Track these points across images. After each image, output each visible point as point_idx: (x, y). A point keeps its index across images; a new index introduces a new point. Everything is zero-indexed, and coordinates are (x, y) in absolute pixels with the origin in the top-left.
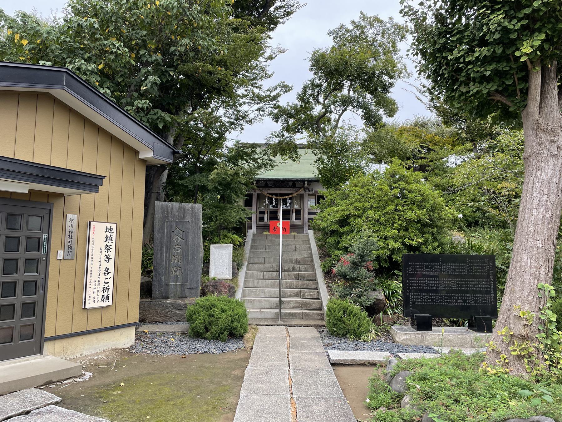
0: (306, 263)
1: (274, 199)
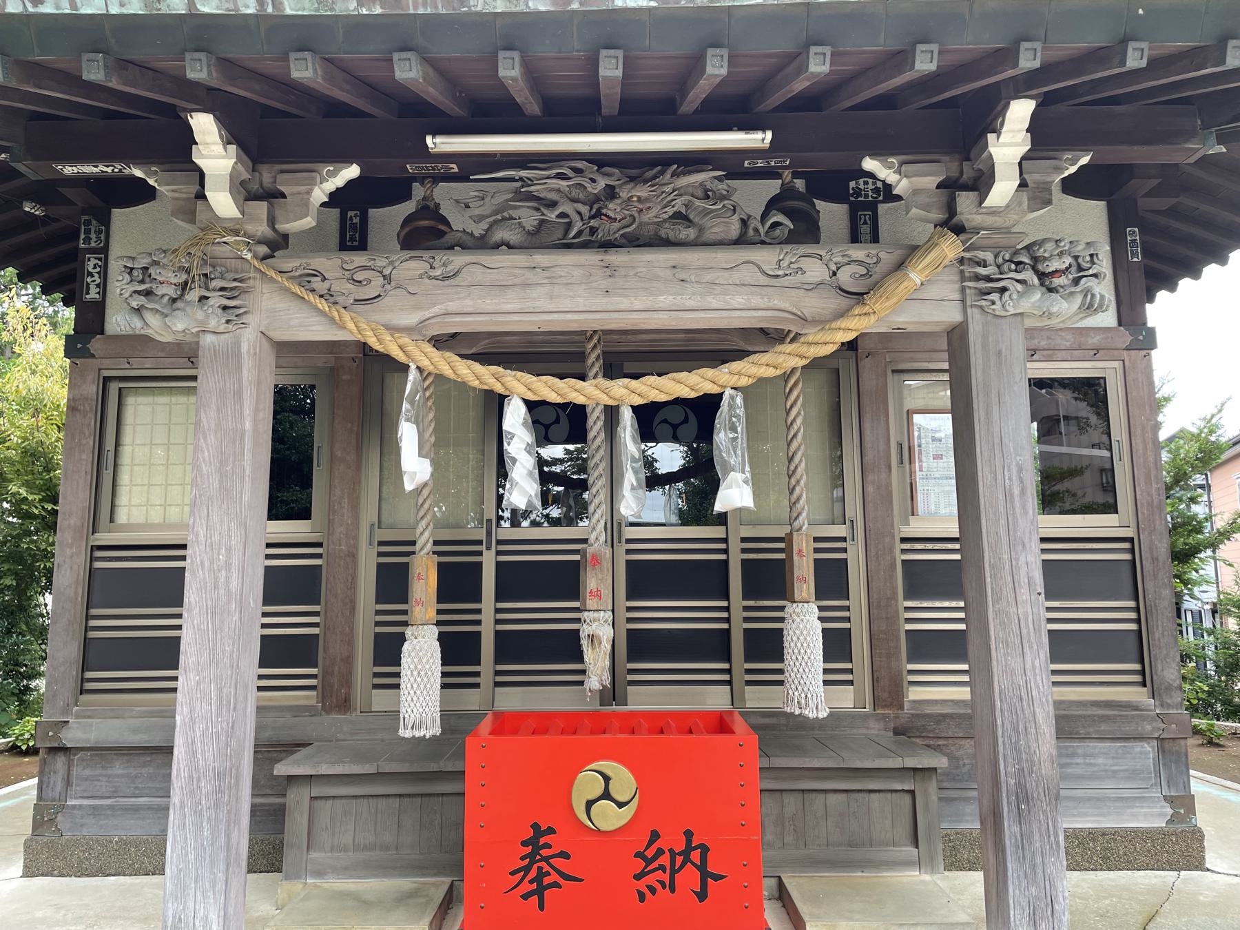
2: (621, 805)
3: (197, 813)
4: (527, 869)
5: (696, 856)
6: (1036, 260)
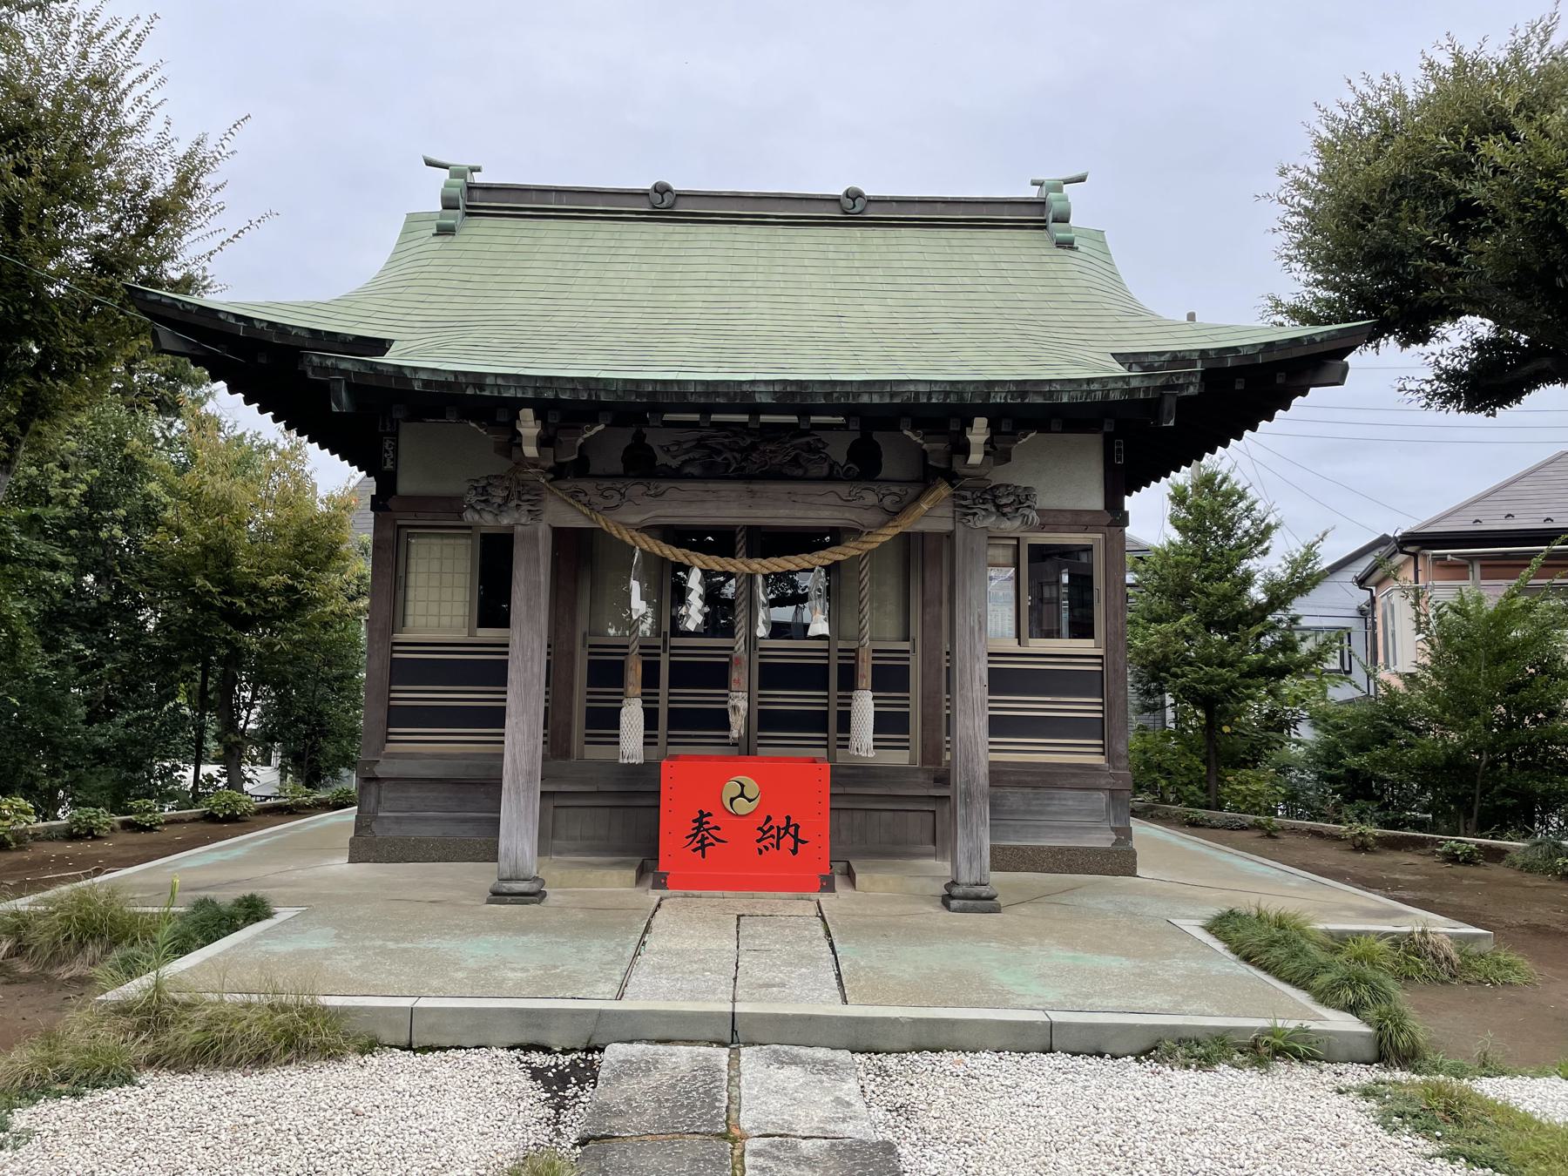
1: (694, 581)
2: (750, 801)
3: (517, 793)
4: (695, 835)
5: (792, 830)
6: (995, 497)
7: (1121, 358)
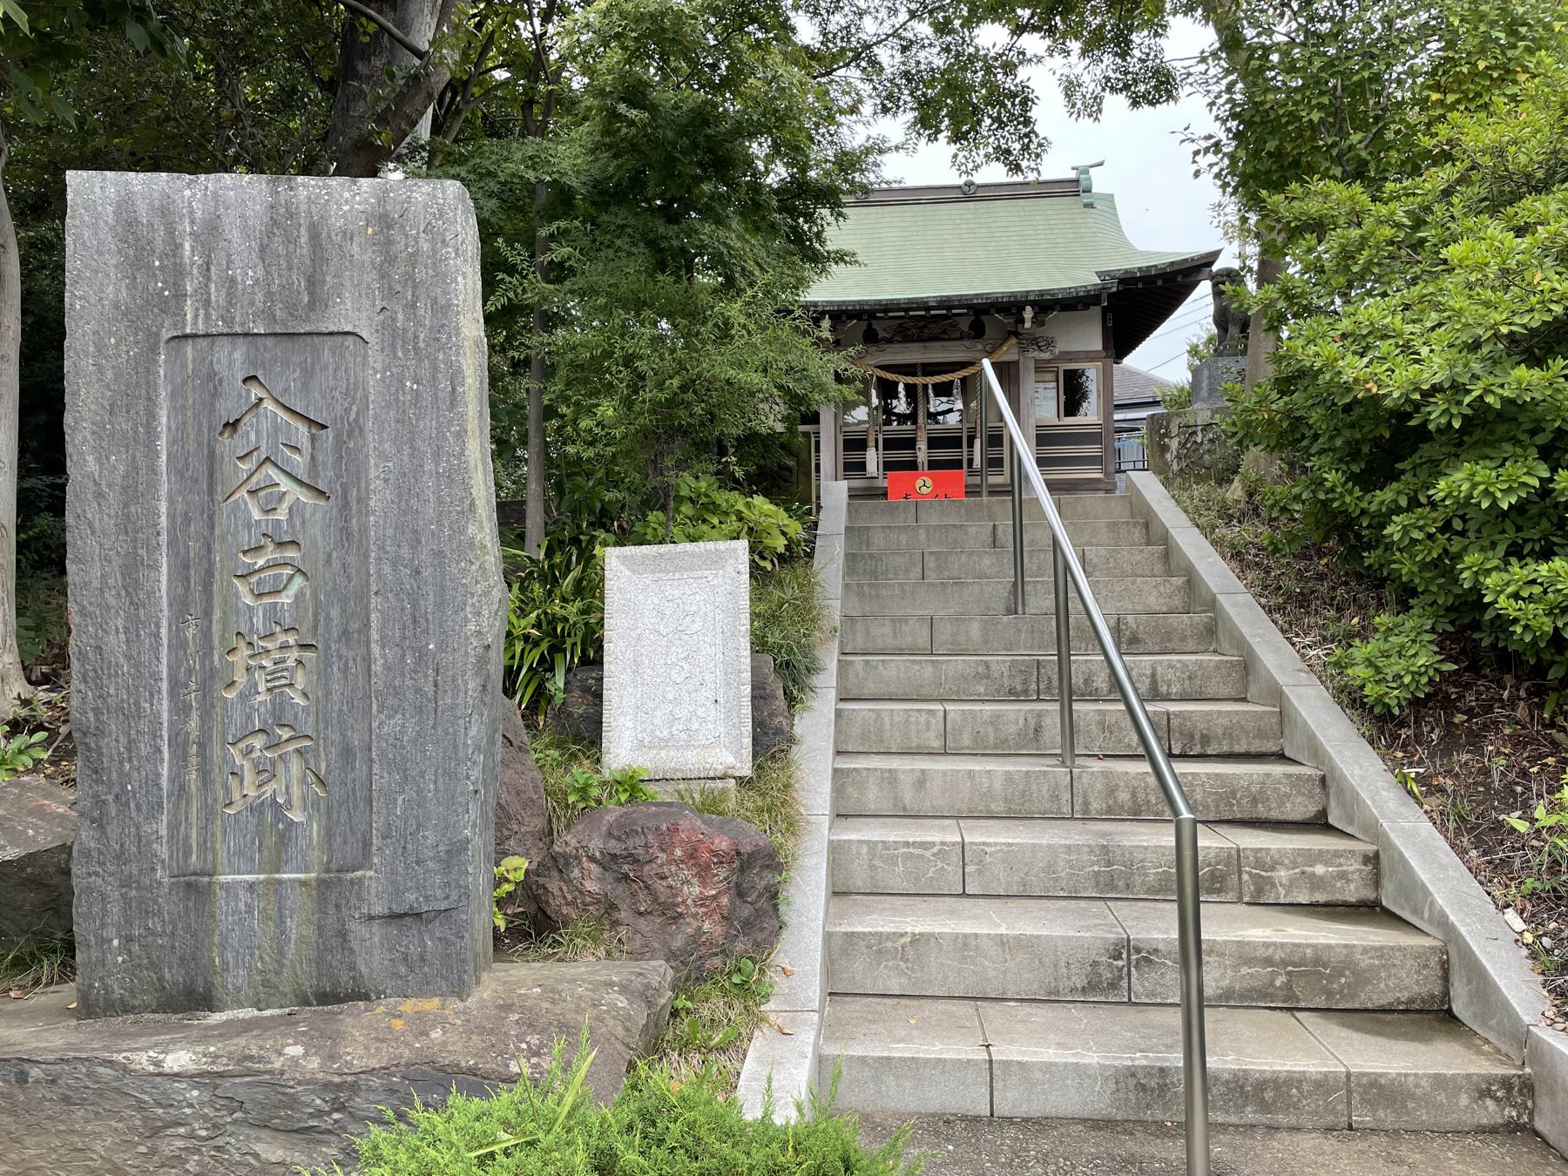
0: (1175, 644)
1: (901, 387)
7: (1099, 274)
